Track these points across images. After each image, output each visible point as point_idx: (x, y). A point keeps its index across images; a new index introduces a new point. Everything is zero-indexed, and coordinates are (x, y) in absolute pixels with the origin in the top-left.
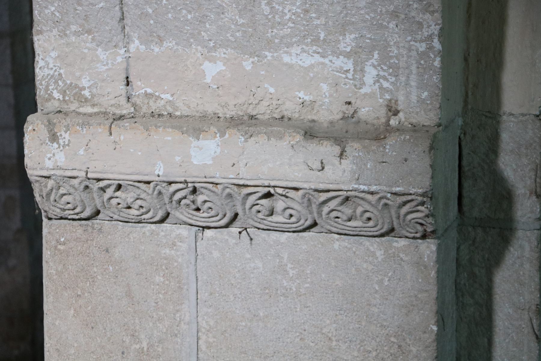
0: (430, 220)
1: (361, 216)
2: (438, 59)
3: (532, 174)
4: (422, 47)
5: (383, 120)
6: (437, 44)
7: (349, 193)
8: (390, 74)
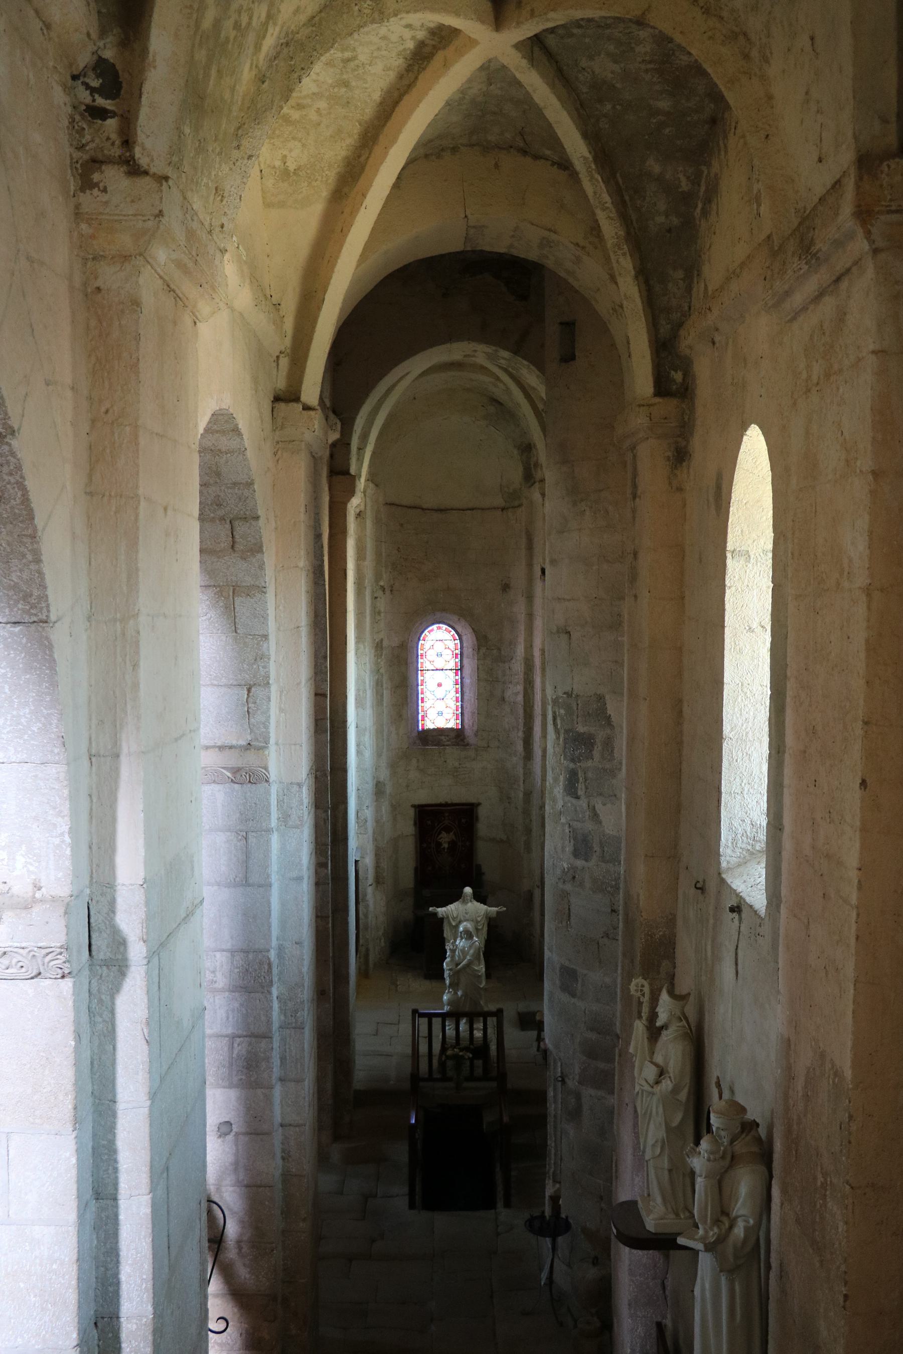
0: (67, 965)
1: (16, 965)
2: (69, 849)
3: (140, 925)
4: (57, 841)
5: (31, 894)
6: (68, 839)
7: (6, 949)
8: (34, 861)
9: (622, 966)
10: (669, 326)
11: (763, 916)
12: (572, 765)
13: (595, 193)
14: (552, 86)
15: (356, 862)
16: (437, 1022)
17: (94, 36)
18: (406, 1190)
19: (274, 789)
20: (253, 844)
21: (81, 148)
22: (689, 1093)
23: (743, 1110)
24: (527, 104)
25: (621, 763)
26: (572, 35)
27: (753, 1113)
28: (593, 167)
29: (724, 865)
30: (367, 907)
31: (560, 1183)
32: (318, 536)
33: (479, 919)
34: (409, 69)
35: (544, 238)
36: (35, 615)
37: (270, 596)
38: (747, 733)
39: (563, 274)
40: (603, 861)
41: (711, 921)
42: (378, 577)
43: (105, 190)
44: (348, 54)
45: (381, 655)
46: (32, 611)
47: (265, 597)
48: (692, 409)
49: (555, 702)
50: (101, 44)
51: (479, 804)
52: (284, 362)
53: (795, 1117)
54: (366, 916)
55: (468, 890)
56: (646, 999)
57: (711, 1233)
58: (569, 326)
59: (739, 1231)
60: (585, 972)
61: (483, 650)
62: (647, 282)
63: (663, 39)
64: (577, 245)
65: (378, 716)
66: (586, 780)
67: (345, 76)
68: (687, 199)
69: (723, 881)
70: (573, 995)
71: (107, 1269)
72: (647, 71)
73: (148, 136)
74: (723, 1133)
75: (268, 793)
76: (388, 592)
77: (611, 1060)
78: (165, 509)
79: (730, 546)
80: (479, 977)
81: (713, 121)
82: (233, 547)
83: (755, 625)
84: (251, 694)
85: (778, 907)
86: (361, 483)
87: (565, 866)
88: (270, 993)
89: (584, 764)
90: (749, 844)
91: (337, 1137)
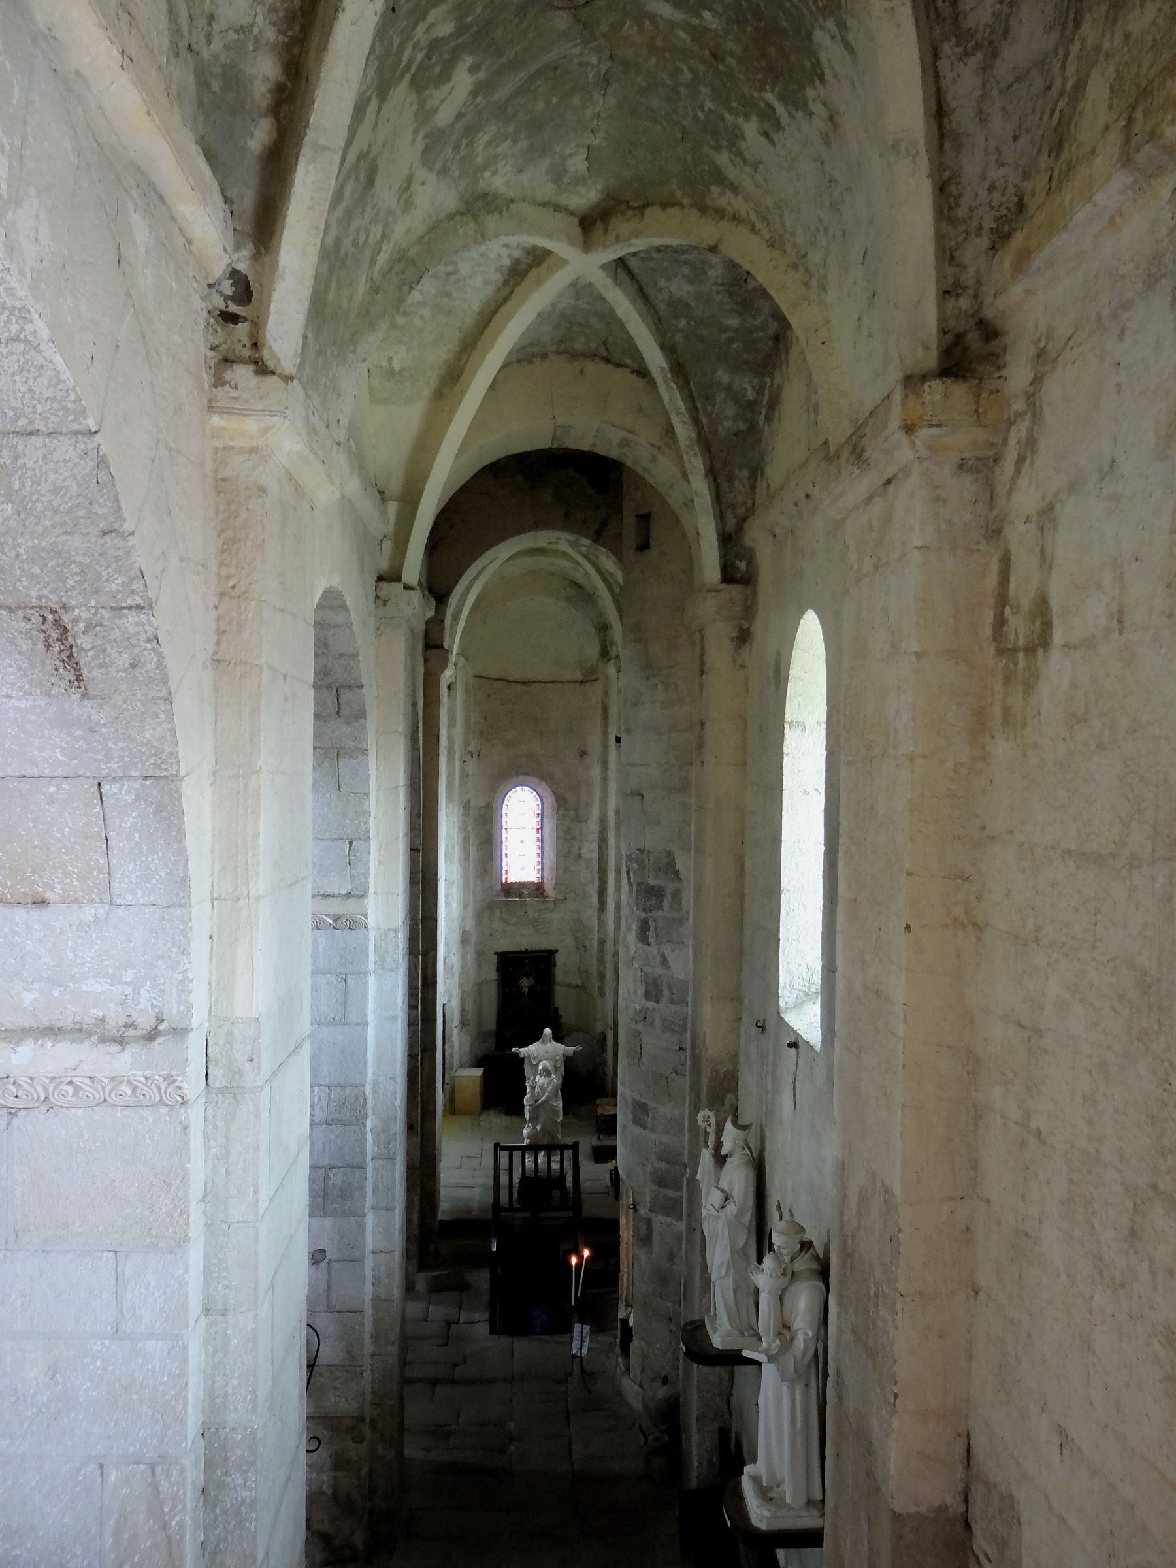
9: (690, 1100)
10: (735, 520)
11: (818, 1051)
12: (643, 915)
13: (670, 399)
14: (634, 302)
15: (444, 1004)
16: (517, 1155)
17: (229, 250)
18: (487, 1315)
19: (372, 935)
20: (352, 986)
21: (214, 348)
22: (752, 1213)
23: (802, 1229)
24: (610, 318)
25: (688, 913)
26: (651, 259)
27: (811, 1235)
28: (669, 376)
29: (782, 1005)
30: (452, 1047)
31: (632, 1306)
32: (414, 705)
33: (557, 1058)
34: (505, 283)
35: (624, 438)
36: (166, 769)
37: (372, 759)
38: (803, 886)
39: (640, 471)
40: (672, 1003)
41: (771, 1058)
42: (466, 743)
43: (236, 387)
44: (450, 268)
45: (469, 814)
46: (163, 766)
47: (367, 759)
48: (754, 594)
49: (629, 857)
50: (235, 257)
51: (557, 951)
52: (388, 545)
53: (850, 1234)
54: (452, 1056)
55: (548, 1031)
56: (712, 1130)
57: (774, 1345)
58: (645, 519)
59: (800, 1342)
60: (655, 1105)
61: (562, 810)
62: (715, 480)
63: (732, 266)
64: (653, 445)
65: (465, 869)
66: (656, 929)
67: (447, 288)
68: (751, 406)
69: (782, 1019)
70: (644, 1127)
71: (214, 1382)
72: (718, 292)
73: (276, 340)
74: (784, 1252)
75: (367, 938)
76: (475, 757)
77: (679, 1188)
78: (285, 677)
79: (788, 718)
80: (558, 1111)
81: (777, 338)
82: (338, 712)
83: (810, 789)
84: (352, 848)
85: (832, 1042)
86: (453, 657)
87: (638, 1007)
88: (365, 1126)
89: (655, 914)
90: (805, 986)
91: (423, 1266)
